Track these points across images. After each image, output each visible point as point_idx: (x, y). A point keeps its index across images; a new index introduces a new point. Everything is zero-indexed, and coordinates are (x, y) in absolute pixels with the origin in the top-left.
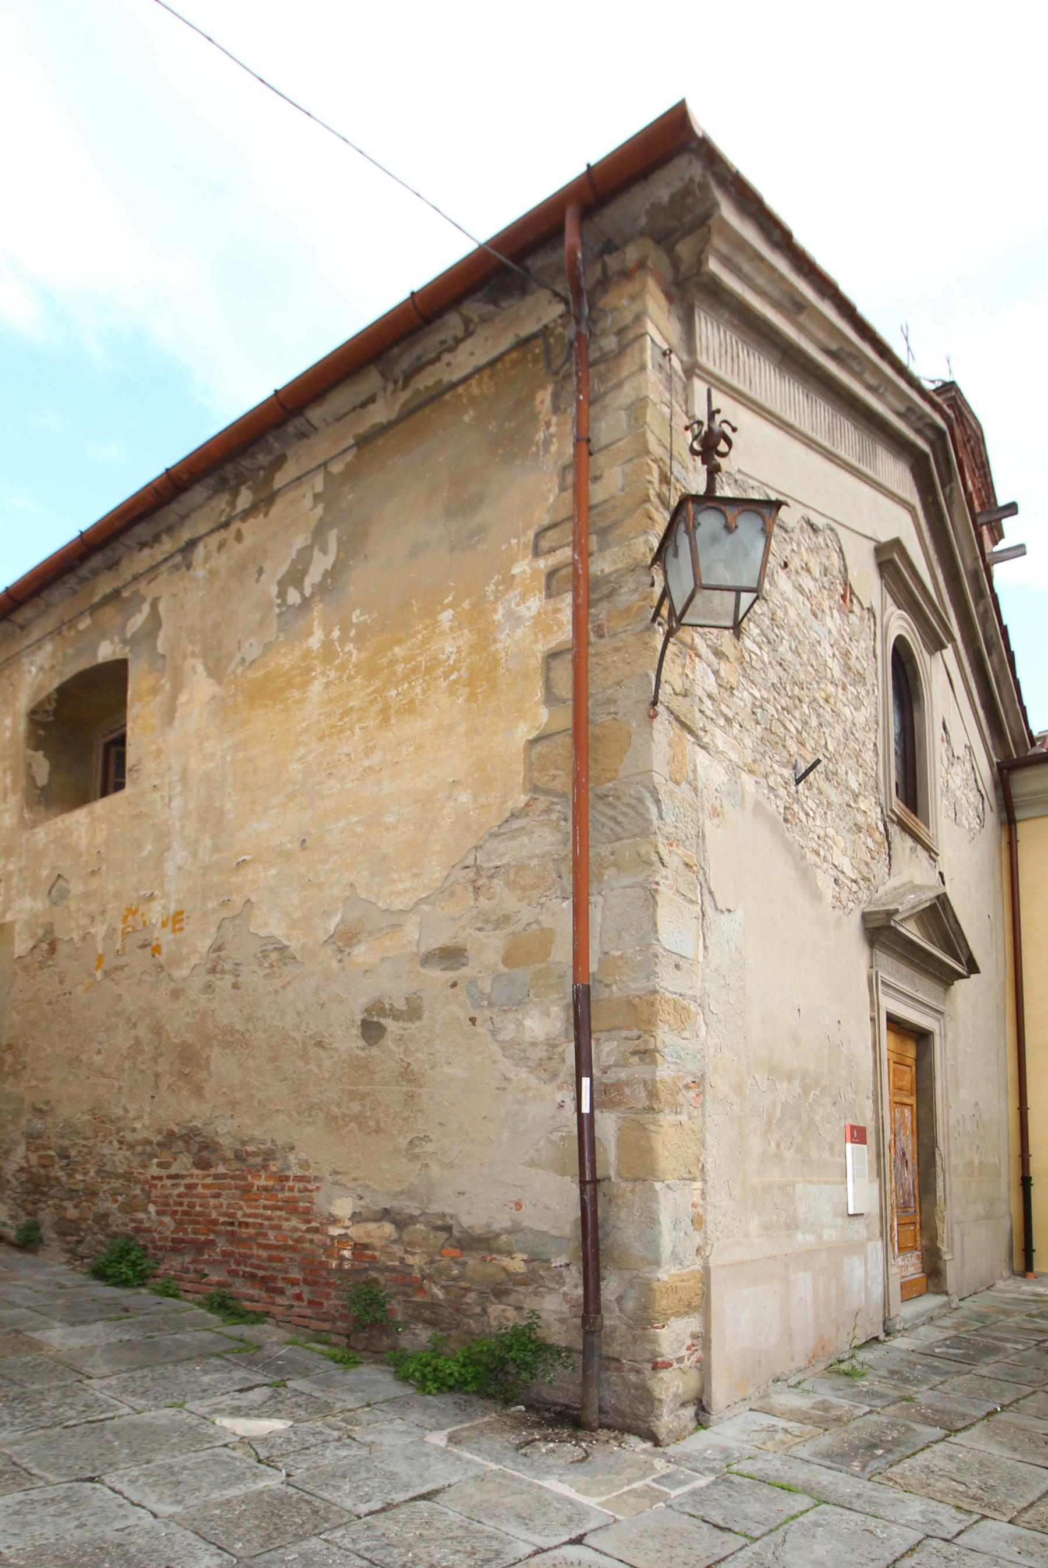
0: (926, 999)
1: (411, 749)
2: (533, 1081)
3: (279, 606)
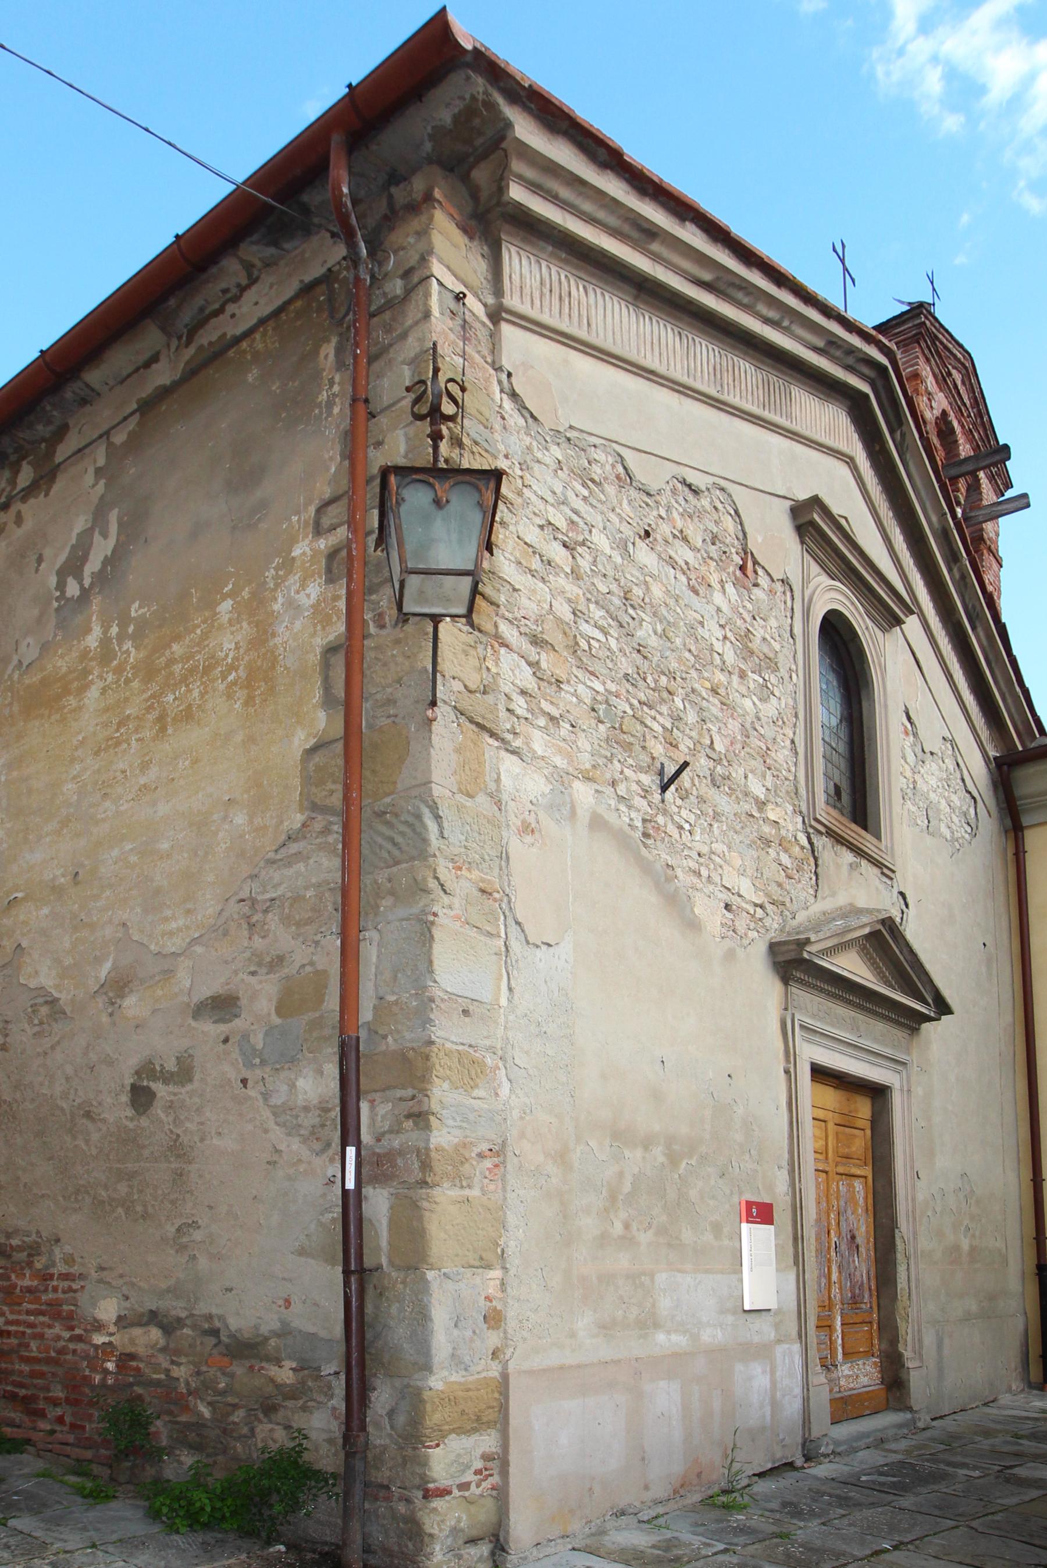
0: (876, 1047)
1: (187, 763)
2: (305, 1154)
3: (57, 599)
